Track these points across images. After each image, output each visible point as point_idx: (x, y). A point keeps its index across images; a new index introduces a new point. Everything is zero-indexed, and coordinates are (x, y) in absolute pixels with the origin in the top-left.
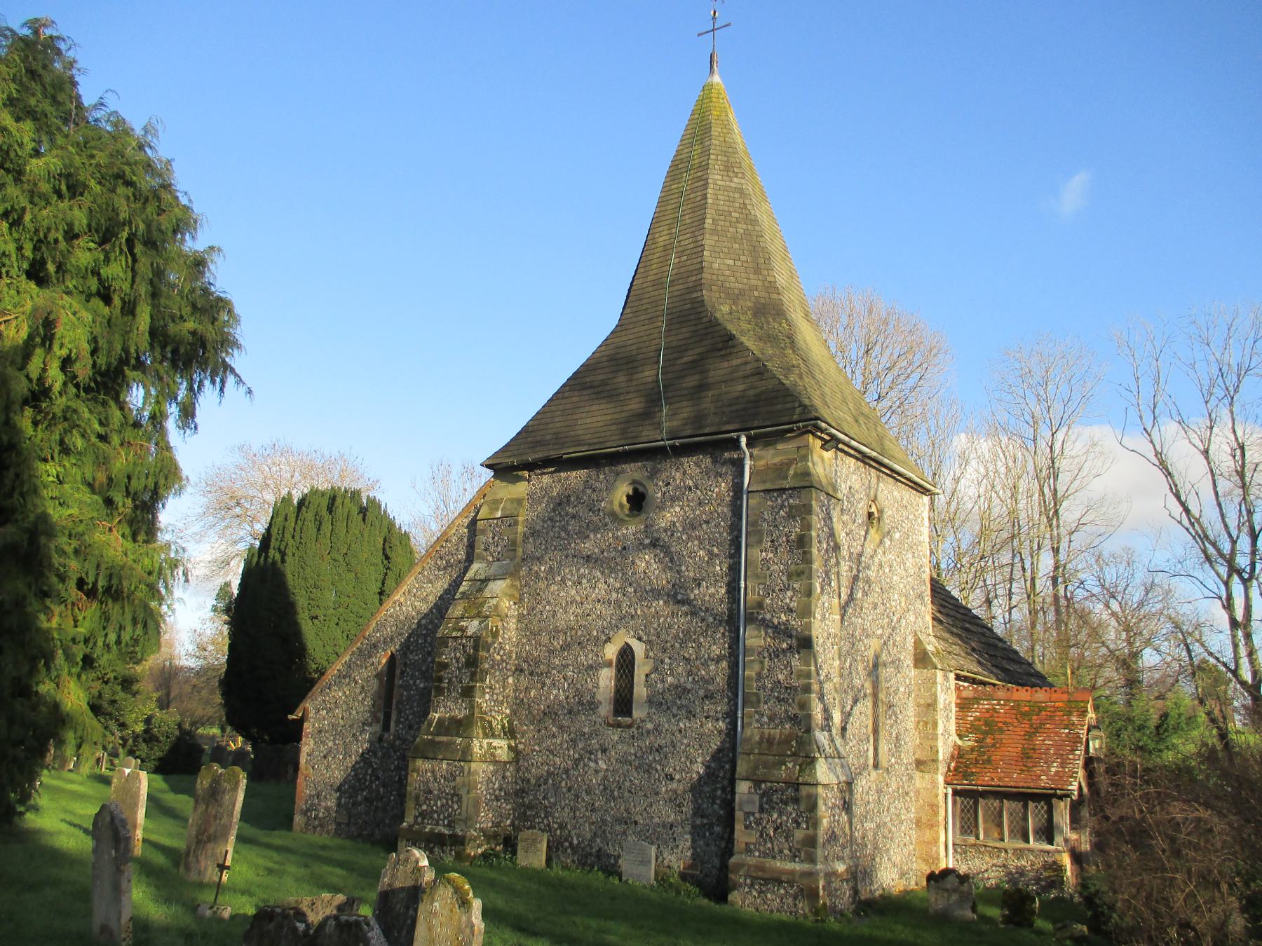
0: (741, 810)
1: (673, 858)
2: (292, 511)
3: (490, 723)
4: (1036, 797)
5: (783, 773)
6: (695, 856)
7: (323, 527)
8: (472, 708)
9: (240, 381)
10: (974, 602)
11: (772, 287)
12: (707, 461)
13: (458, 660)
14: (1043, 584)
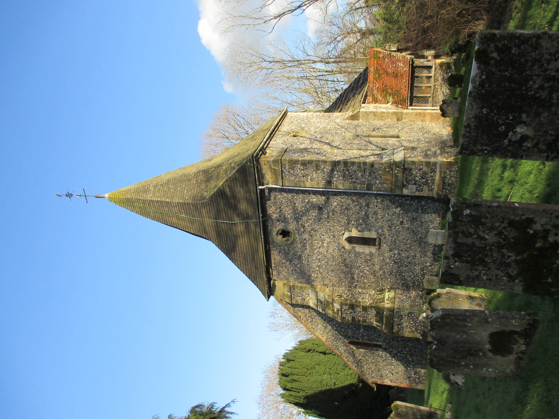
0: (415, 193)
2: (287, 393)
3: (378, 299)
4: (413, 72)
6: (434, 213)
7: (295, 379)
9: (228, 405)
10: (335, 96)
11: (196, 174)
13: (351, 313)
14: (330, 67)
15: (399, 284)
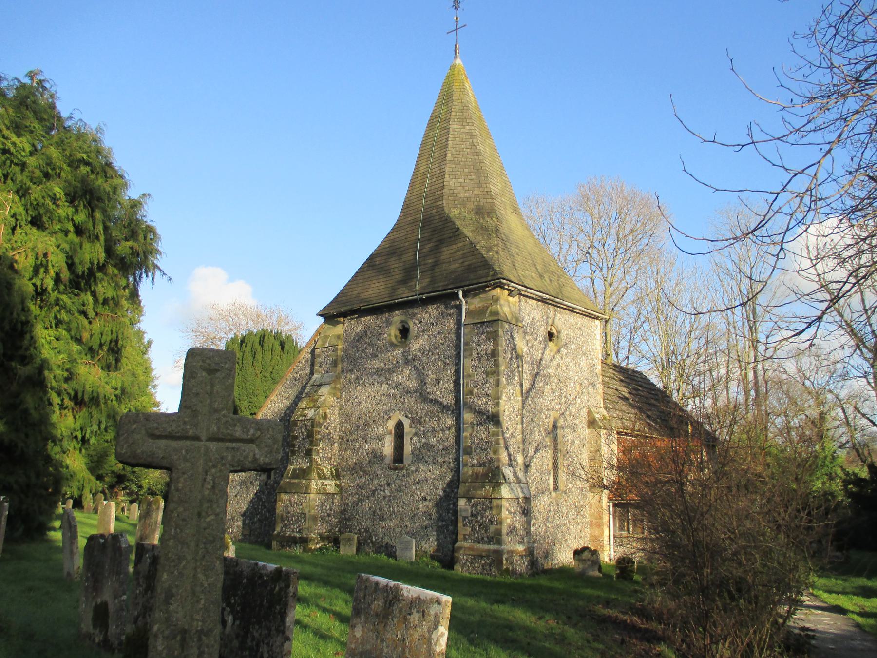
1: (427, 546)
3: (323, 471)
5: (482, 492)
6: (438, 546)
8: (311, 462)
9: (163, 273)
11: (488, 194)
12: (442, 308)
15: (347, 498)
